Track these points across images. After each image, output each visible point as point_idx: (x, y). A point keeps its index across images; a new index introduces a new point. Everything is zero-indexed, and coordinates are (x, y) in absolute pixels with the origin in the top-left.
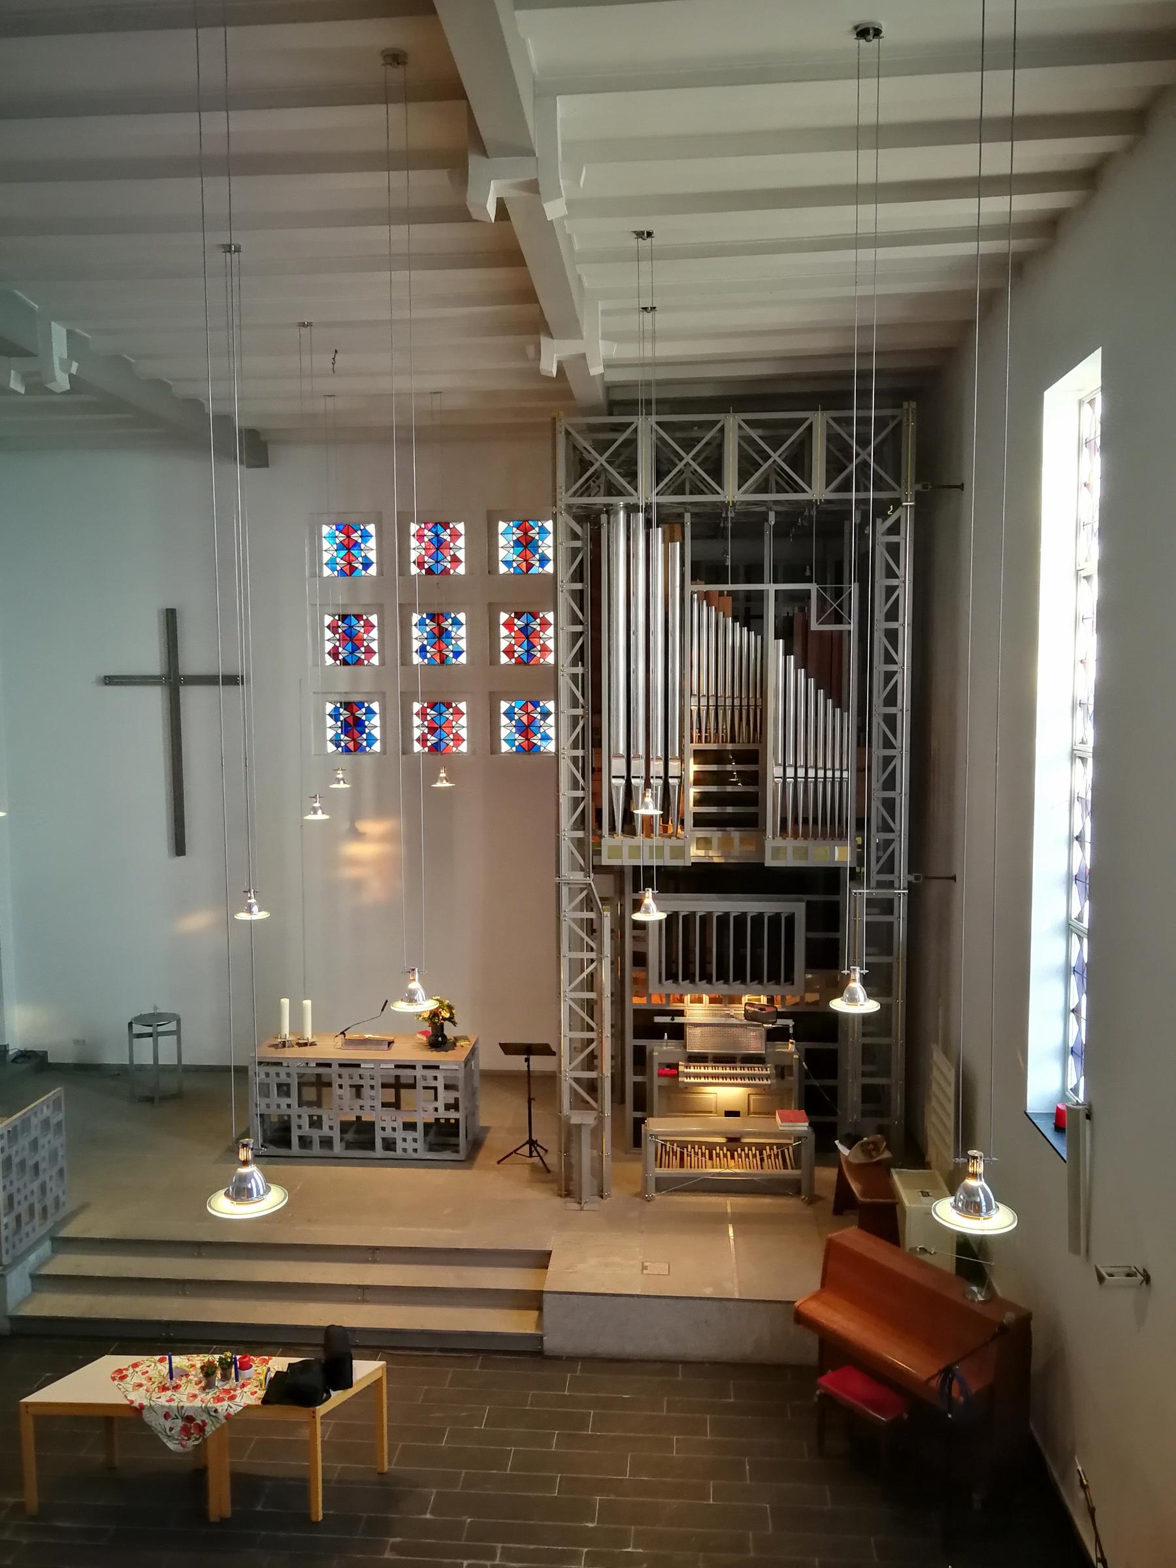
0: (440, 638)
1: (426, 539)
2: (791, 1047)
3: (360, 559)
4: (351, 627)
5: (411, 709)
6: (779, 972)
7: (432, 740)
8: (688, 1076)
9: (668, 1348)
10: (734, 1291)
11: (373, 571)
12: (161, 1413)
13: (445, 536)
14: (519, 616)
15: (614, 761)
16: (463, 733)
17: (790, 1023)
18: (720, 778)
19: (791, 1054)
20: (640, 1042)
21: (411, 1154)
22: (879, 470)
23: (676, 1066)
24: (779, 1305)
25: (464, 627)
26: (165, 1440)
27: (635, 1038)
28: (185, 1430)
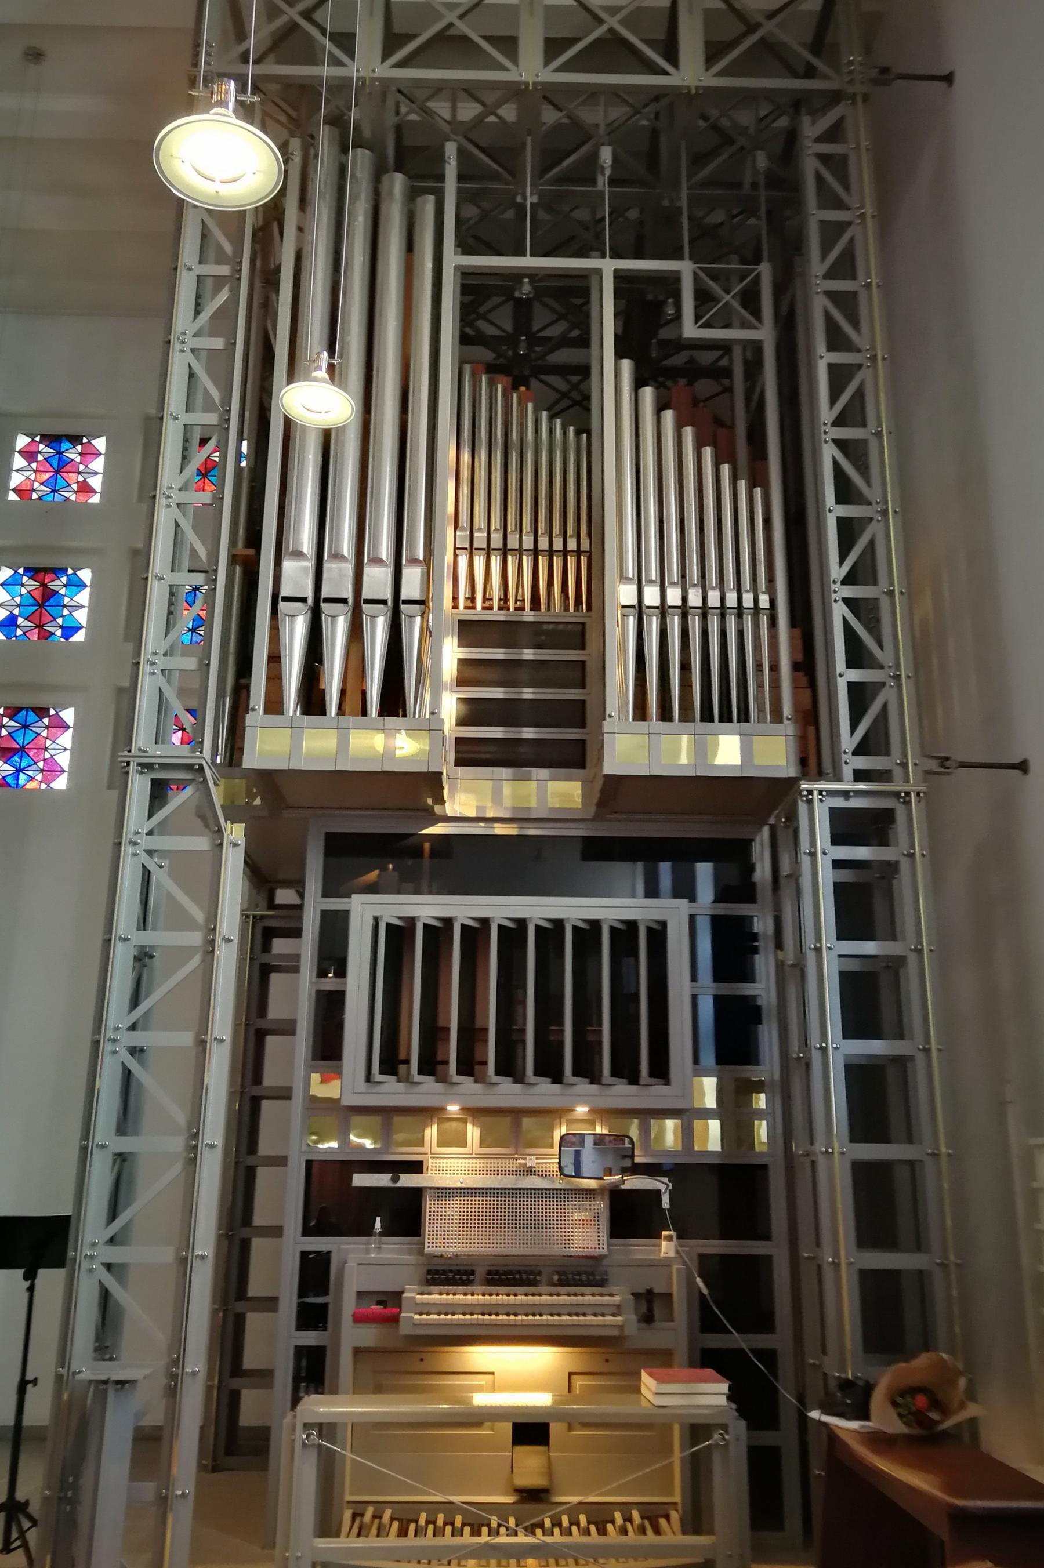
0: (42, 606)
2: (667, 1247)
6: (638, 1054)
8: (425, 1309)
10: (557, 806)
15: (288, 565)
16: (64, 760)
17: (660, 1184)
18: (507, 672)
19: (666, 1263)
23: (398, 1295)
25: (87, 590)
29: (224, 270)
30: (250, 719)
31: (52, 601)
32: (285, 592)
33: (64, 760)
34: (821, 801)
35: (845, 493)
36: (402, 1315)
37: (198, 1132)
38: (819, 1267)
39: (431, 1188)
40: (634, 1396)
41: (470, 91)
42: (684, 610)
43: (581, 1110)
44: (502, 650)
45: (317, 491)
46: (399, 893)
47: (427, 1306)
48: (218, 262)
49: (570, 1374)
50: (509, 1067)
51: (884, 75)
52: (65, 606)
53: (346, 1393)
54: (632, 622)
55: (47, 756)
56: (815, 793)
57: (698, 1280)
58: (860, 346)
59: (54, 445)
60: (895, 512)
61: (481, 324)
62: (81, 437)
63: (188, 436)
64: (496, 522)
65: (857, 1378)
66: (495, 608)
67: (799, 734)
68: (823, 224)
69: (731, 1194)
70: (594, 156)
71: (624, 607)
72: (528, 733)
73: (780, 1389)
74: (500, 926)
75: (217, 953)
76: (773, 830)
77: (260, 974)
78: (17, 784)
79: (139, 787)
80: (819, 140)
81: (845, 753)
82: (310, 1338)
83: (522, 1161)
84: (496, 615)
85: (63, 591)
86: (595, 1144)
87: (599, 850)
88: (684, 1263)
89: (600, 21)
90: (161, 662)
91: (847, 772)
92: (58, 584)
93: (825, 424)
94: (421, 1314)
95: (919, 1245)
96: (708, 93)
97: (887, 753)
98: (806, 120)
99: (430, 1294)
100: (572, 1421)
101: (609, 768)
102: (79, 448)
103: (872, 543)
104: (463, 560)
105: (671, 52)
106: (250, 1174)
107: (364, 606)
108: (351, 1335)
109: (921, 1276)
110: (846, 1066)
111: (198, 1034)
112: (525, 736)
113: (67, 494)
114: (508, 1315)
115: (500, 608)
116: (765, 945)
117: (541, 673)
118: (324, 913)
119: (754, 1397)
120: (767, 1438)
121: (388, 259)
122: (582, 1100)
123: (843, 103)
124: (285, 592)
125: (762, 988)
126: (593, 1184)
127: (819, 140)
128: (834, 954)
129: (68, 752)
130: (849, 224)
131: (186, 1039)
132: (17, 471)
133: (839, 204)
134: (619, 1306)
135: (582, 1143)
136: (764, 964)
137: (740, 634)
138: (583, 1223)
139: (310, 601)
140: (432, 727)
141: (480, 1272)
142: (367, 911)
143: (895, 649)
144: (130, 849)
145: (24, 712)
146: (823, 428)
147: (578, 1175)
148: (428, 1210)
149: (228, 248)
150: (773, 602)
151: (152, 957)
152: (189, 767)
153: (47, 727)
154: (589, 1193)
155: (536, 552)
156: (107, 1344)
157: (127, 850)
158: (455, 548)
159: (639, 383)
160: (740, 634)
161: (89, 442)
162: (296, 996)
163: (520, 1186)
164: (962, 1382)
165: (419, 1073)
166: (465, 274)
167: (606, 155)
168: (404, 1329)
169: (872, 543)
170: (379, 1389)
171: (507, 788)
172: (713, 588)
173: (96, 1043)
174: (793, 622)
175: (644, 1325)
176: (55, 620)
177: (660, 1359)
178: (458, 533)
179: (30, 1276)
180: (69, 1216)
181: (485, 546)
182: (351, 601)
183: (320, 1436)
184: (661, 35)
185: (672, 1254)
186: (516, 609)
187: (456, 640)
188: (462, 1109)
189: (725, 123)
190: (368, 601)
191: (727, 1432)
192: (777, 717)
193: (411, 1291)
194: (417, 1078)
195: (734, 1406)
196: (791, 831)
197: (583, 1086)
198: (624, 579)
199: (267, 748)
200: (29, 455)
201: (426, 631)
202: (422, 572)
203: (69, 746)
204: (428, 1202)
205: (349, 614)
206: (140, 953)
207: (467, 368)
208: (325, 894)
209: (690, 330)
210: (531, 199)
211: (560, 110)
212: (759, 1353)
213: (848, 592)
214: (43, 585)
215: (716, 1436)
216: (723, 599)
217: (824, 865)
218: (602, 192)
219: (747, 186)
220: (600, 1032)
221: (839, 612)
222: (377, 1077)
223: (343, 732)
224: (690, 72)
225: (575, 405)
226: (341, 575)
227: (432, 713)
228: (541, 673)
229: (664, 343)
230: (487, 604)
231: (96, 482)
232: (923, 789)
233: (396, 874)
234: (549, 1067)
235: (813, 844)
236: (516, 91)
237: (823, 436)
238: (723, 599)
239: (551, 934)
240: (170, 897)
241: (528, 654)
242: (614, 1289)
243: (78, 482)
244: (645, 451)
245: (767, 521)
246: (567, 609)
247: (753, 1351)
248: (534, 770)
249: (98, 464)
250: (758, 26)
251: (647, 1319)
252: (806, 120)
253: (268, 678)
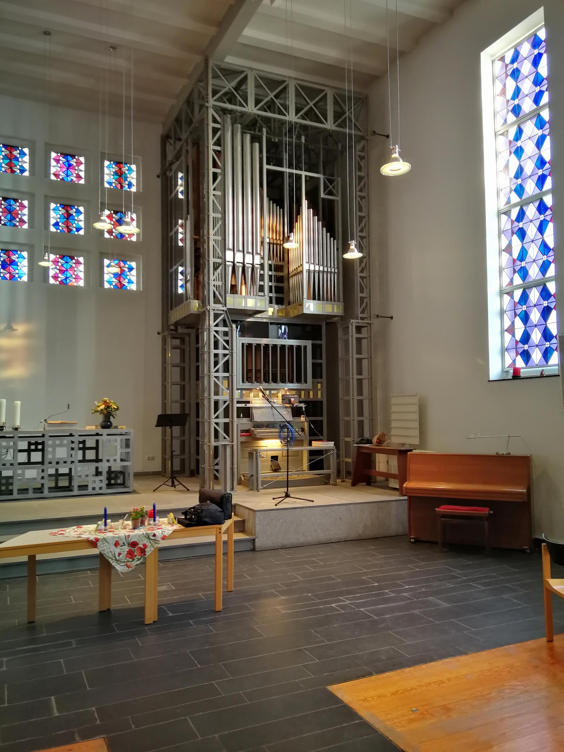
1: (61, 162)
2: (303, 419)
3: (18, 167)
4: (10, 205)
7: (61, 277)
9: (323, 537)
11: (26, 174)
12: (113, 542)
13: (73, 162)
14: (116, 212)
17: (303, 405)
19: (303, 422)
21: (97, 491)
22: (356, 123)
24: (375, 504)
26: (114, 564)
27: (321, 345)
28: (130, 554)
31: (71, 218)
43: (286, 389)
62: (75, 156)
92: (73, 212)
166: (268, 170)
179: (171, 428)
200: (57, 161)
214: (67, 211)
221: (211, 153)
234: (275, 381)
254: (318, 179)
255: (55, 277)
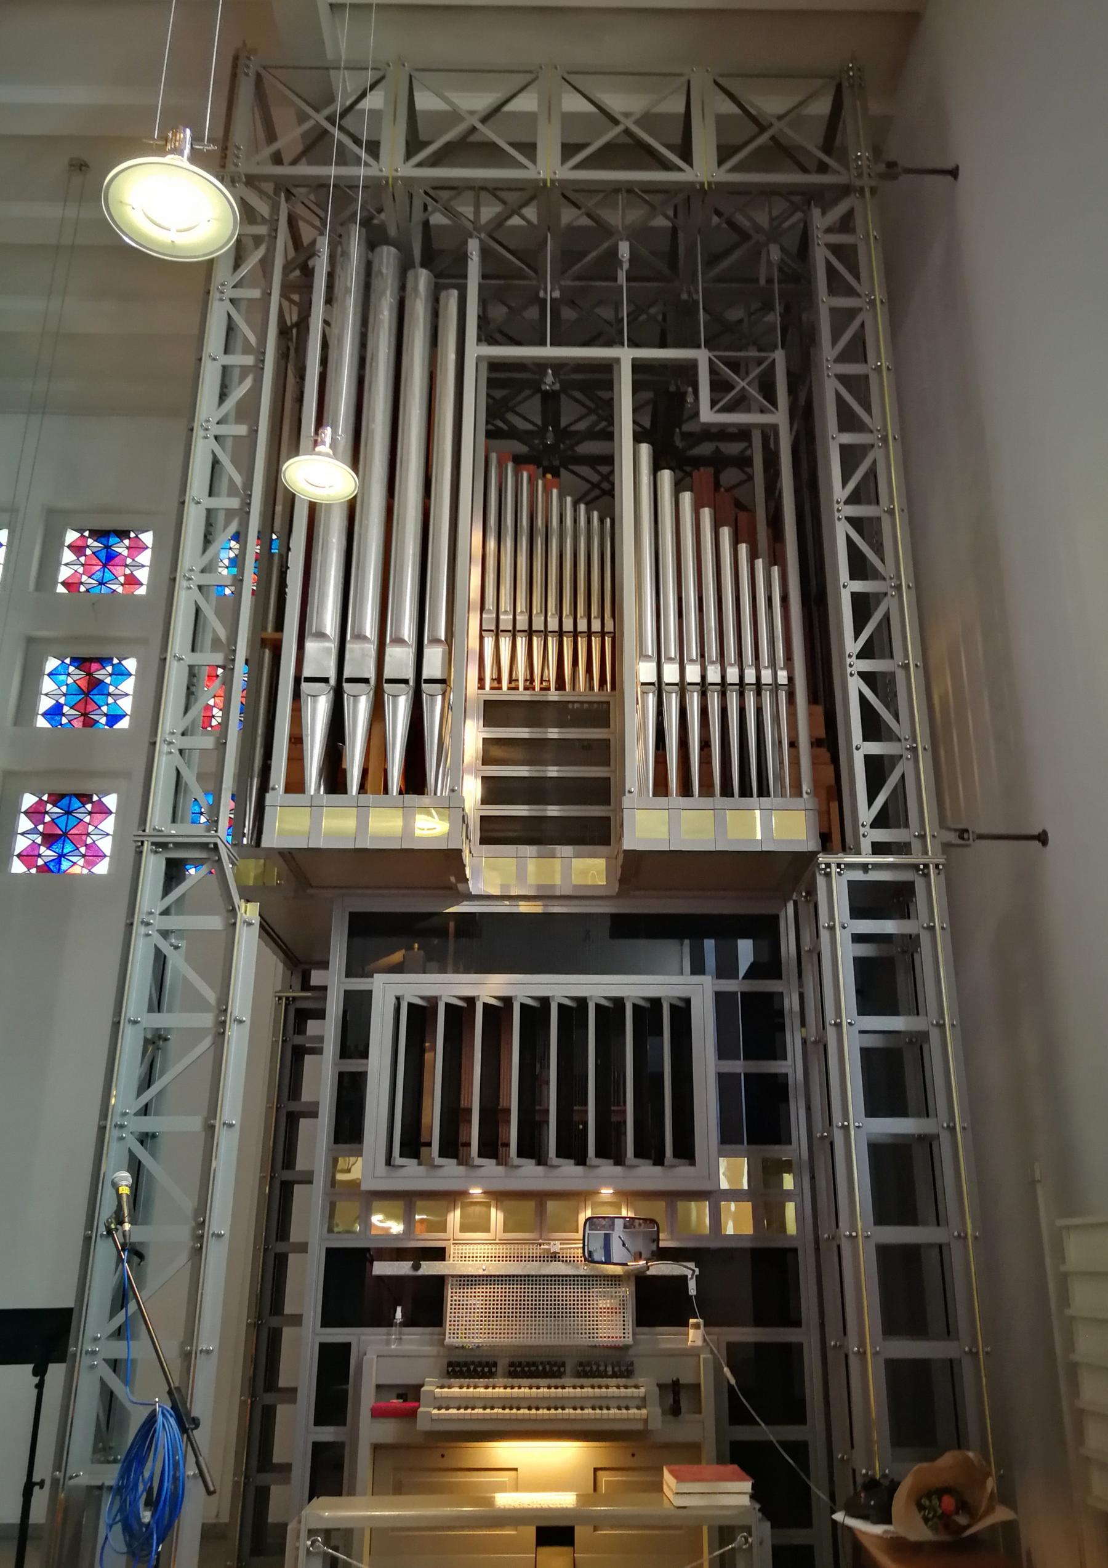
2: (694, 1335)
5: (18, 803)
6: (661, 1135)
8: (444, 1403)
16: (106, 845)
17: (687, 1269)
18: (534, 751)
19: (694, 1353)
20: (337, 1335)
29: (249, 360)
30: (269, 797)
32: (307, 672)
33: (106, 845)
34: (839, 873)
35: (859, 568)
36: (421, 1409)
37: (204, 1221)
38: (847, 1356)
39: (453, 1276)
40: (655, 1496)
41: (494, 190)
42: (703, 686)
43: (606, 1192)
44: (527, 730)
45: (341, 574)
46: (424, 973)
47: (447, 1400)
48: (245, 352)
49: (596, 1470)
50: (531, 1149)
51: (892, 170)
52: (109, 694)
53: (365, 1494)
54: (651, 700)
55: (89, 841)
56: (833, 866)
57: (726, 1370)
58: (871, 427)
59: (104, 540)
60: (909, 587)
61: (595, 478)
63: (212, 521)
64: (521, 606)
65: (884, 1476)
66: (521, 688)
67: (817, 807)
68: (833, 310)
69: (764, 1280)
70: (614, 252)
71: (643, 684)
72: (553, 811)
73: (813, 1487)
74: (523, 1005)
75: (228, 1033)
76: (795, 903)
77: (294, 1056)
78: (59, 869)
79: (153, 867)
80: (829, 230)
81: (863, 825)
82: (328, 1434)
83: (546, 1247)
84: (522, 695)
85: (108, 680)
86: (625, 1227)
87: (626, 927)
88: (712, 1352)
89: (616, 122)
90: (180, 742)
91: (866, 845)
92: (103, 674)
93: (838, 502)
94: (439, 1409)
95: (949, 1332)
96: (720, 188)
97: (907, 825)
98: (816, 212)
99: (449, 1387)
100: (597, 1522)
101: (628, 844)
102: (127, 542)
103: (887, 618)
104: (489, 642)
105: (686, 152)
106: (281, 1262)
107: (385, 685)
108: (370, 1431)
109: (951, 1365)
110: (869, 1145)
111: (206, 1119)
112: (550, 814)
113: (114, 587)
114: (530, 1408)
115: (526, 688)
116: (791, 1023)
117: (564, 751)
118: (348, 994)
119: (782, 1492)
120: (797, 1537)
121: (413, 353)
122: (607, 1181)
123: (852, 195)
124: (307, 672)
125: (791, 1066)
126: (618, 1270)
127: (829, 230)
128: (855, 1030)
129: (110, 838)
130: (861, 309)
131: (194, 1124)
132: (66, 565)
133: (851, 292)
134: (644, 1399)
135: (612, 1226)
136: (793, 1041)
137: (759, 711)
138: (611, 1310)
139: (333, 682)
140: (452, 806)
141: (503, 1365)
142: (390, 991)
143: (911, 720)
144: (143, 930)
145: (68, 798)
146: (836, 506)
147: (608, 1261)
148: (449, 1298)
149: (252, 339)
150: (791, 679)
151: (166, 1039)
152: (204, 846)
153: (90, 813)
154: (615, 1280)
155: (560, 633)
156: (112, 1445)
157: (139, 930)
158: (481, 630)
159: (656, 468)
160: (759, 711)
161: (137, 536)
162: (321, 1079)
163: (544, 1272)
164: (991, 1484)
165: (440, 1156)
167: (624, 250)
168: (422, 1425)
169: (887, 618)
170: (398, 1489)
171: (531, 866)
172: (732, 665)
173: (102, 1129)
174: (813, 698)
175: (670, 1417)
176: (100, 708)
177: (685, 1454)
178: (484, 616)
179: (40, 1372)
180: (72, 1309)
181: (510, 628)
182: (373, 681)
183: (327, 1542)
184: (677, 139)
185: (699, 1343)
186: (541, 689)
187: (481, 723)
188: (484, 1193)
189: (740, 219)
190: (389, 681)
191: (751, 1535)
192: (797, 791)
193: (431, 1384)
194: (439, 1161)
195: (758, 1506)
196: (812, 906)
197: (607, 1168)
198: (643, 656)
199: (287, 827)
200: (78, 549)
201: (447, 707)
202: (443, 652)
203: (111, 832)
204: (450, 1291)
205: (372, 693)
206: (154, 1036)
207: (494, 457)
208: (349, 974)
209: (707, 415)
210: (550, 293)
211: (579, 208)
212: (788, 1446)
213: (865, 665)
214: (89, 674)
215: (740, 1539)
216: (742, 677)
217: (843, 939)
218: (622, 286)
219: (762, 282)
220: (624, 1112)
221: (855, 685)
222: (398, 1160)
223: (362, 811)
224: (704, 168)
225: (601, 495)
226: (364, 655)
227: (453, 790)
228: (564, 751)
229: (686, 436)
230: (513, 685)
231: (143, 575)
232: (942, 861)
233: (422, 952)
234: (572, 1148)
235: (832, 917)
236: (535, 191)
237: (837, 514)
238: (742, 677)
239: (611, 1013)
240: (185, 979)
241: (553, 733)
242: (641, 1381)
243: (125, 575)
244: (664, 534)
245: (785, 599)
246: (591, 688)
247: (781, 1443)
248: (558, 848)
249: (145, 558)
250: (771, 125)
251: (675, 1411)
252: (816, 212)
253: (289, 759)
254: (693, 365)
255: (28, 857)
